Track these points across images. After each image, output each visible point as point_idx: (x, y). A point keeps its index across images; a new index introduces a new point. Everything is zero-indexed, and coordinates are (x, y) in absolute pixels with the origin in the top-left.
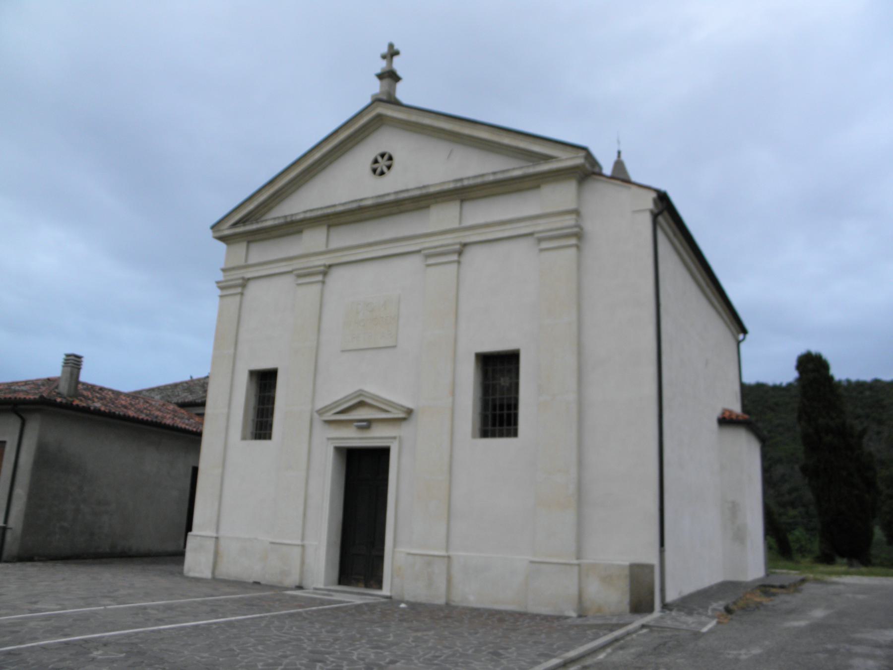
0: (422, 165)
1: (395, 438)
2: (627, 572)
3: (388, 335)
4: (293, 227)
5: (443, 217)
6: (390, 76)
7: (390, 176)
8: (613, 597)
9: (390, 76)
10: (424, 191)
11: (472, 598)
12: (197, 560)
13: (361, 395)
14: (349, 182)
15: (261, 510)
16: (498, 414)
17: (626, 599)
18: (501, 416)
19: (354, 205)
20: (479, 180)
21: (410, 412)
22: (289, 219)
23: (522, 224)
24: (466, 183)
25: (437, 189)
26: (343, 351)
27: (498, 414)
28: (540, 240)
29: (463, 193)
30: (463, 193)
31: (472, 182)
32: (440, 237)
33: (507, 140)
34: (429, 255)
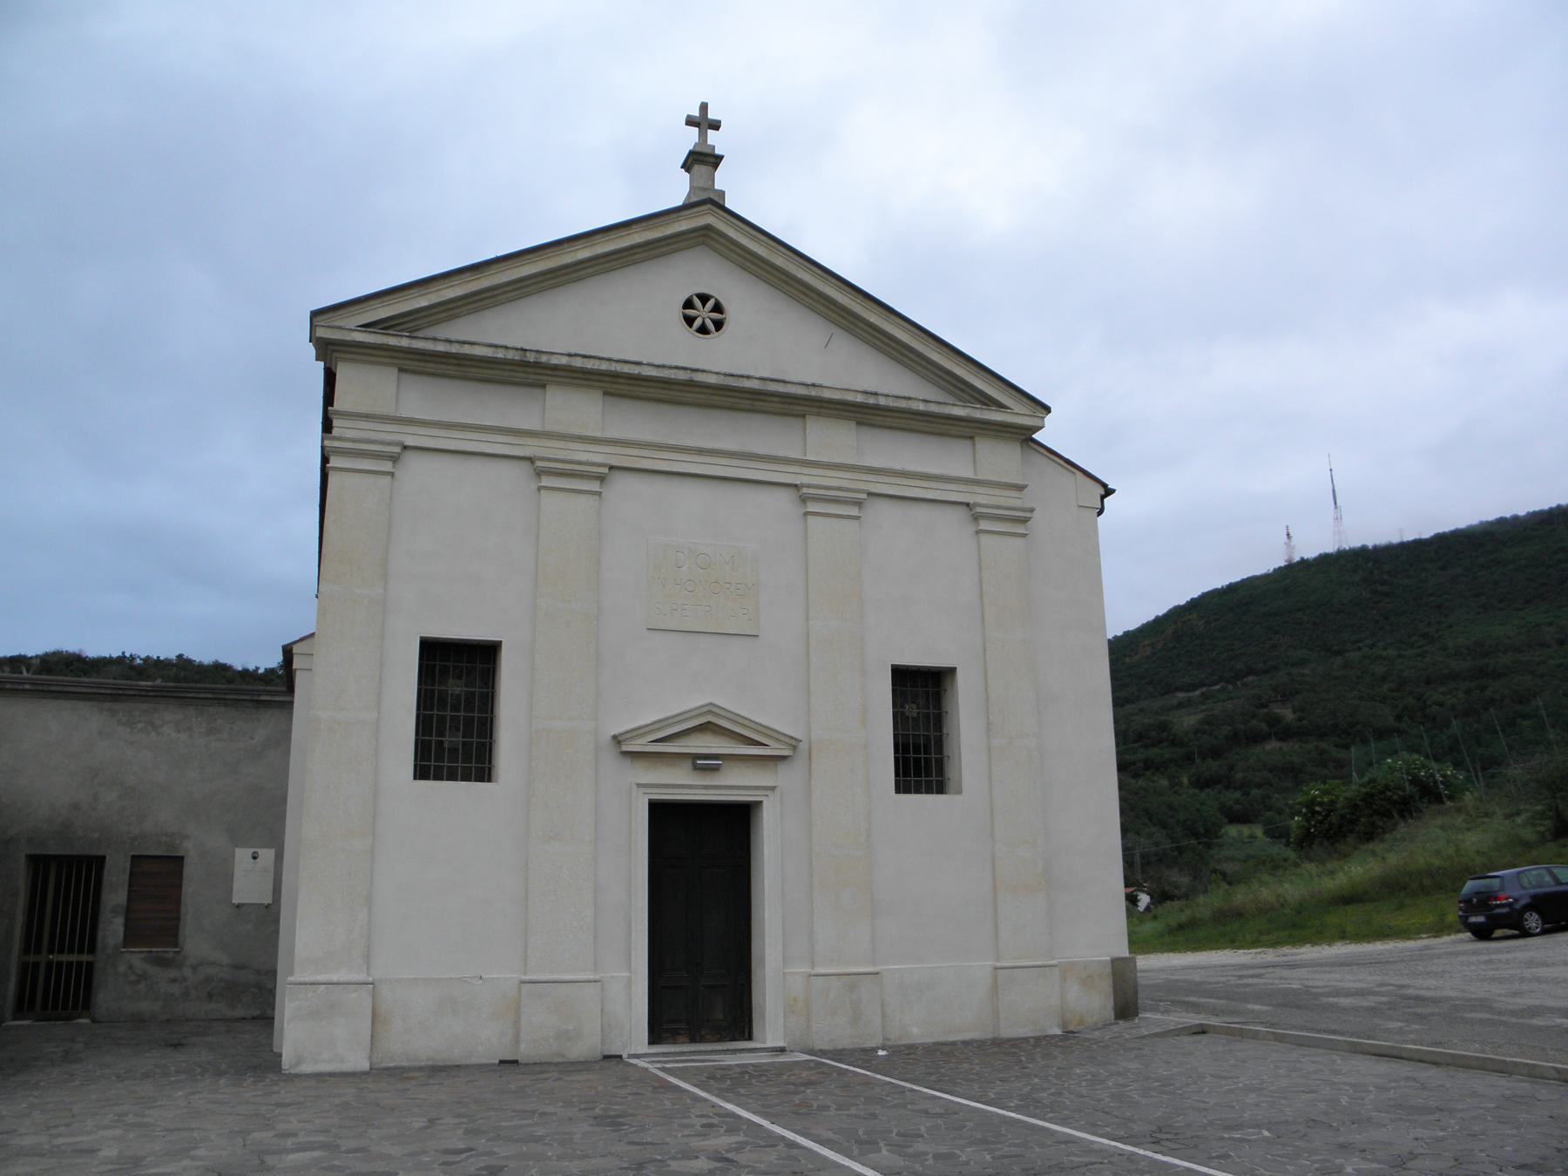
0: (767, 341)
1: (773, 788)
2: (1108, 969)
3: (676, 612)
4: (528, 372)
5: (830, 441)
6: (702, 160)
7: (715, 339)
8: (1096, 1003)
9: (702, 160)
10: (813, 393)
11: (915, 1030)
12: (311, 1035)
13: (710, 712)
14: (635, 322)
15: (443, 924)
16: (921, 761)
17: (1110, 1003)
18: (917, 761)
19: (682, 375)
20: (903, 404)
21: (794, 743)
22: (531, 358)
23: (953, 487)
24: (882, 401)
25: (837, 396)
26: (313, 635)
27: (921, 761)
28: (540, 473)
29: (866, 414)
30: (866, 414)
31: (891, 403)
32: (962, 488)
33: (935, 356)
34: (540, 470)
